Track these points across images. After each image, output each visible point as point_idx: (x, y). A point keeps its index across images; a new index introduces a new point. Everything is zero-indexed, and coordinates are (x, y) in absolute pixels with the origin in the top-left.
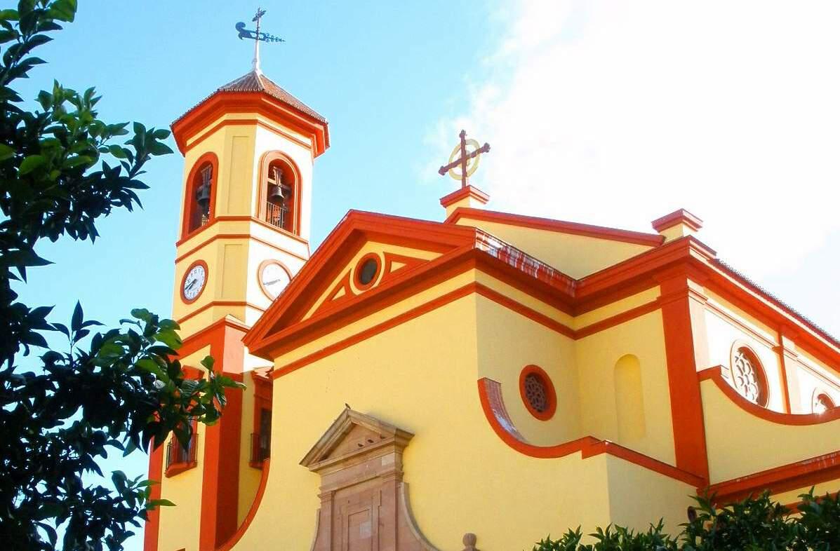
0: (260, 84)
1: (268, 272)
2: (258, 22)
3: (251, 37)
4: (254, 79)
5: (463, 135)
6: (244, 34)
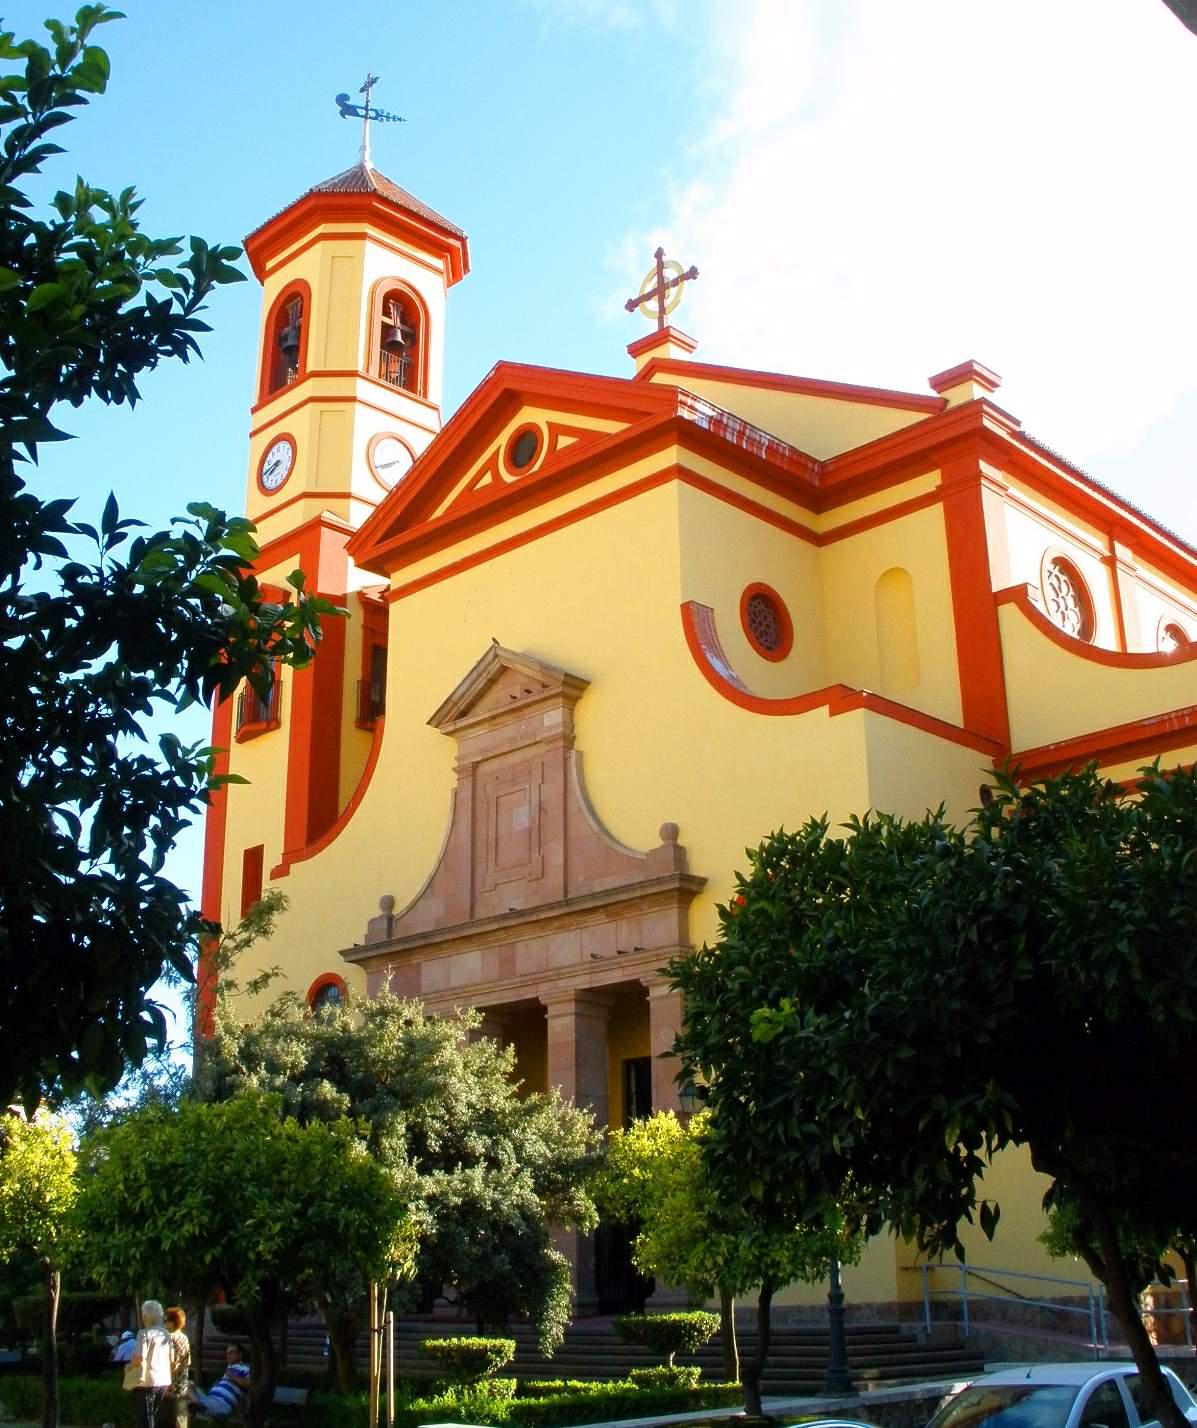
5: (659, 254)
6: (348, 110)
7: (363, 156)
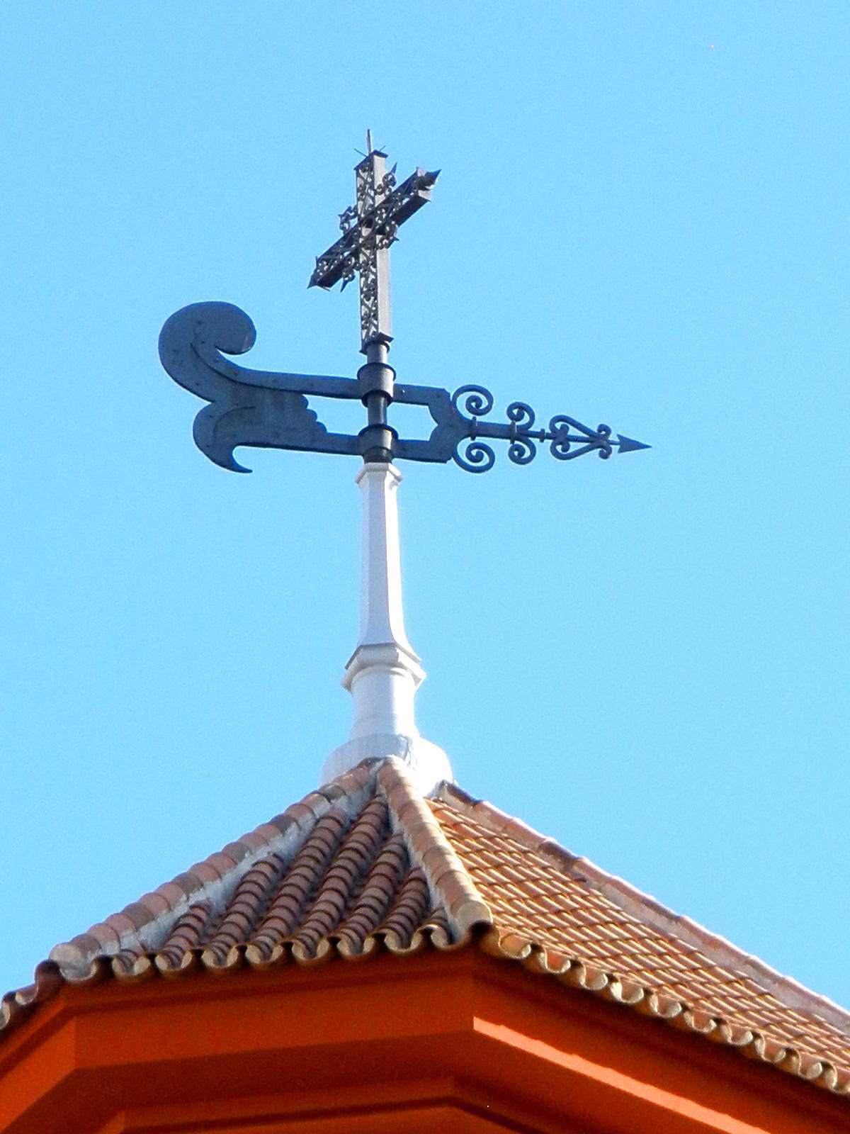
0: (448, 877)
1: (236, 374)
2: (370, 291)
3: (315, 439)
4: (386, 824)
6: (243, 407)
7: (381, 708)
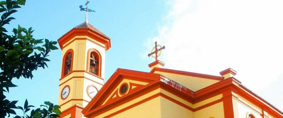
6: (82, 9)
